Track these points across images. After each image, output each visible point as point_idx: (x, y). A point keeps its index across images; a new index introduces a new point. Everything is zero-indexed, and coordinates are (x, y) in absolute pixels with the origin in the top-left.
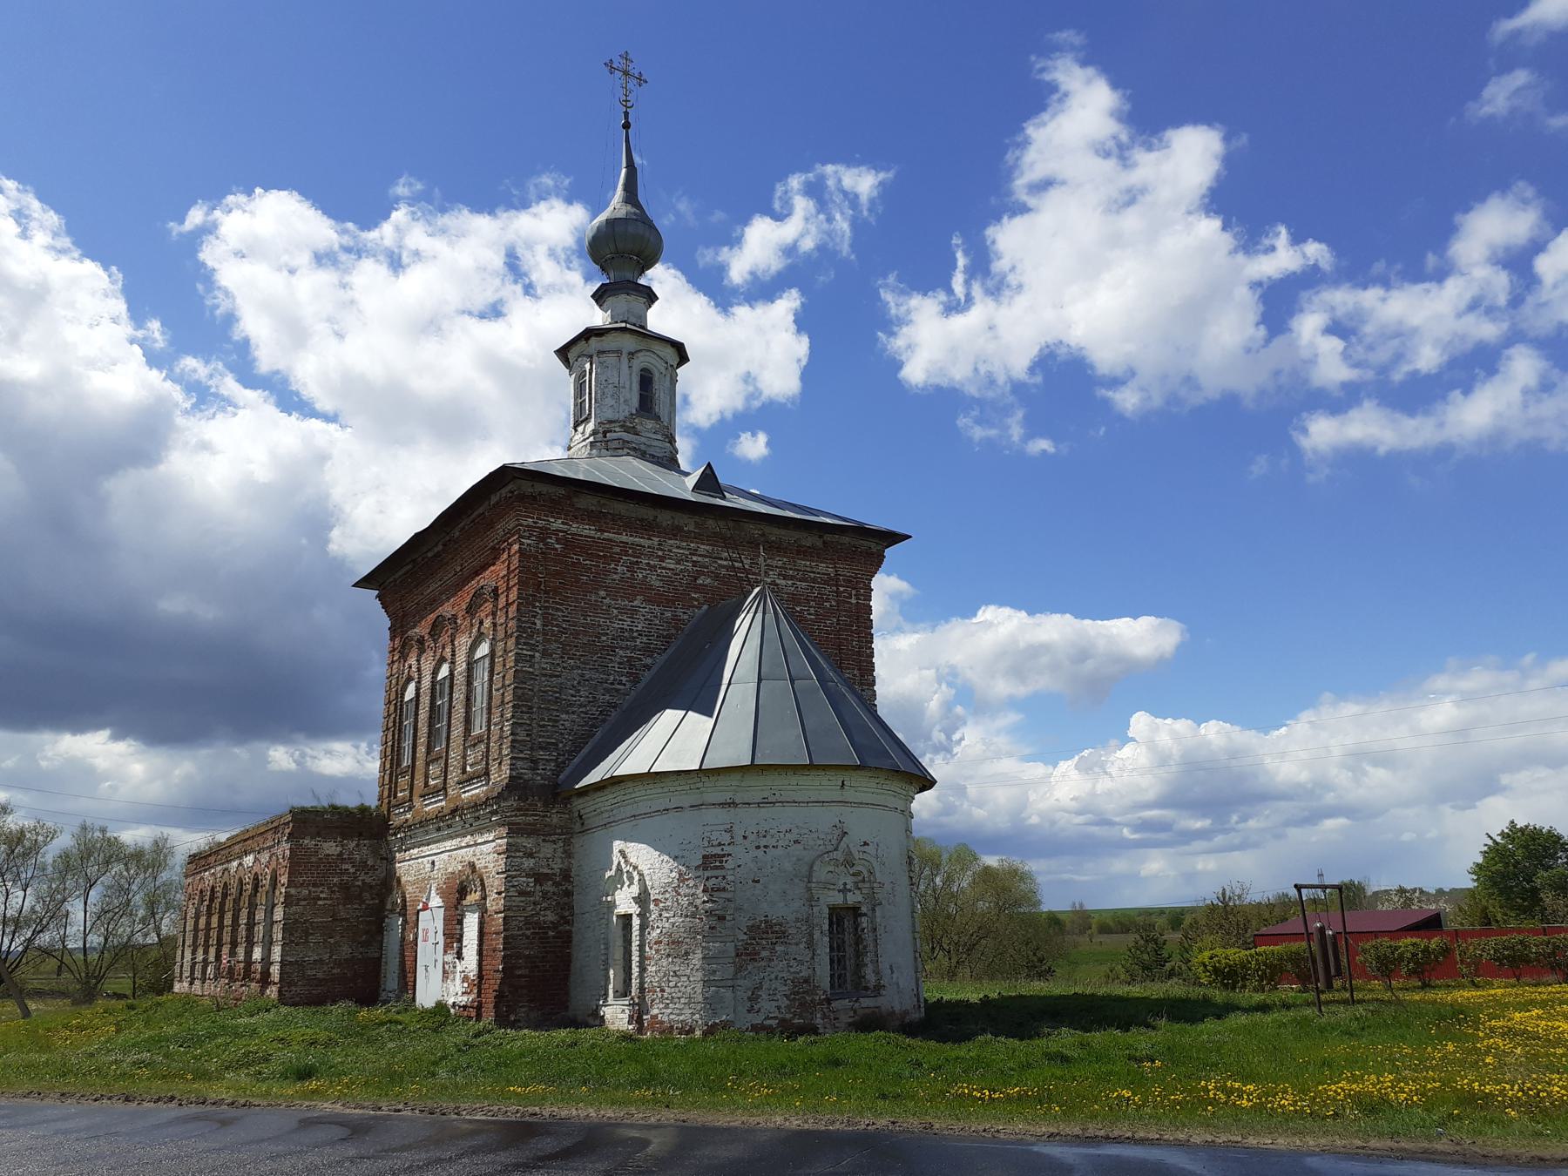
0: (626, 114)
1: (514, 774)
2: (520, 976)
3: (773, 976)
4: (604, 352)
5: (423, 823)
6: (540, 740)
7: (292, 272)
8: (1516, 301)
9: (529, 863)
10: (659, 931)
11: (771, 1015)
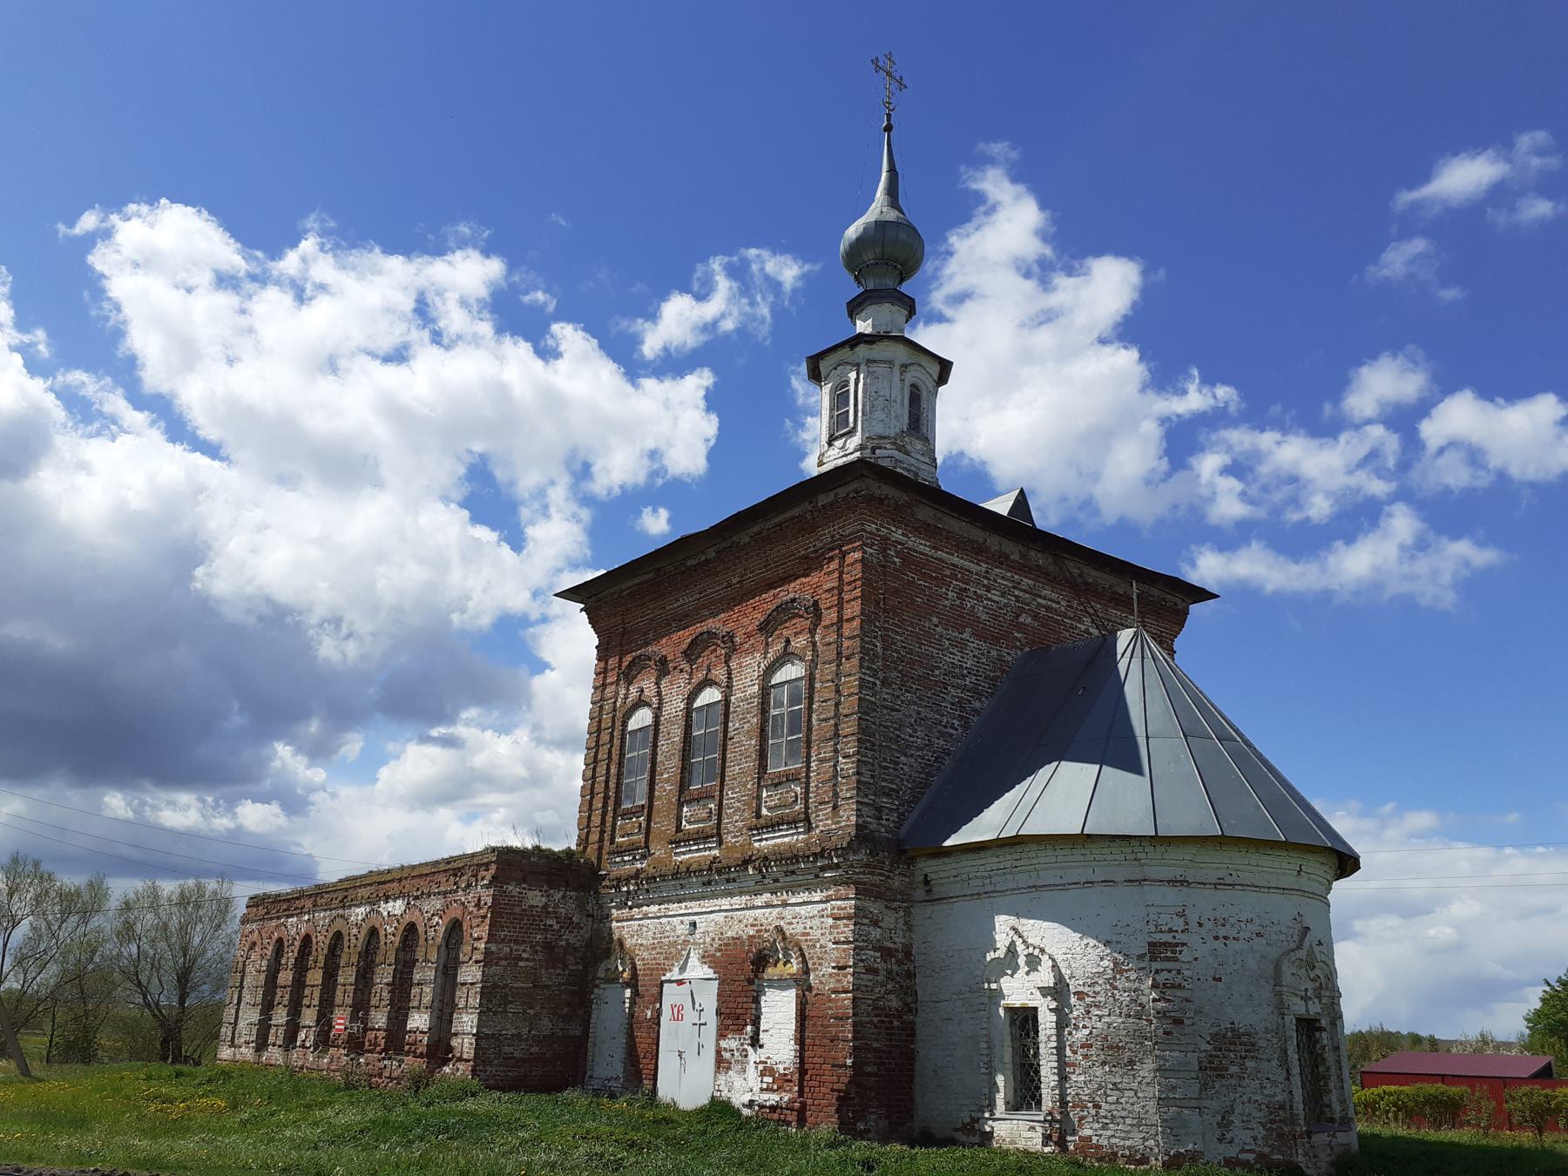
0: (889, 116)
1: (860, 822)
2: (870, 1075)
3: (1245, 1099)
4: (875, 361)
5: (681, 875)
6: (883, 784)
7: (189, 290)
8: (1404, 466)
9: (875, 933)
10: (1087, 1032)
11: (1247, 1148)
